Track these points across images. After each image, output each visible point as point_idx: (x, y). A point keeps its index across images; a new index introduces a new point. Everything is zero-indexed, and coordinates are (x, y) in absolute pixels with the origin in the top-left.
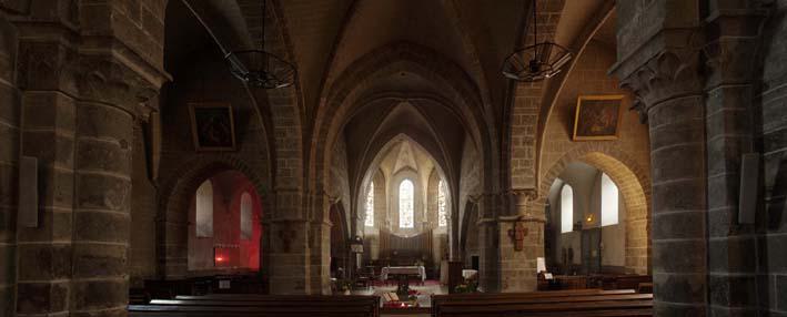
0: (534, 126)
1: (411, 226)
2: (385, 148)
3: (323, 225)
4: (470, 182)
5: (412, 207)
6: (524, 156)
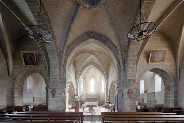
0: (136, 58)
1: (94, 91)
2: (86, 70)
3: (65, 90)
4: (113, 77)
6: (132, 68)
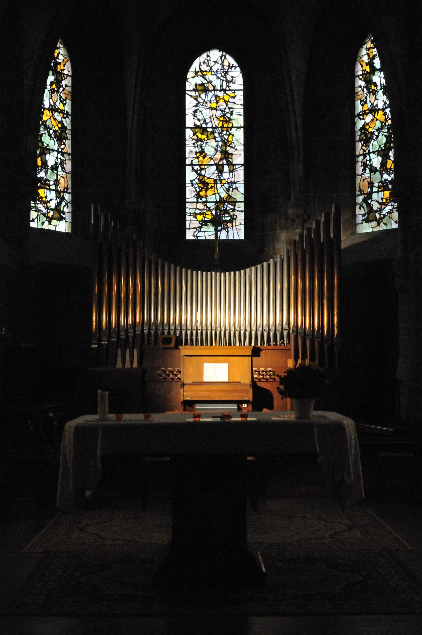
5: (239, 158)
